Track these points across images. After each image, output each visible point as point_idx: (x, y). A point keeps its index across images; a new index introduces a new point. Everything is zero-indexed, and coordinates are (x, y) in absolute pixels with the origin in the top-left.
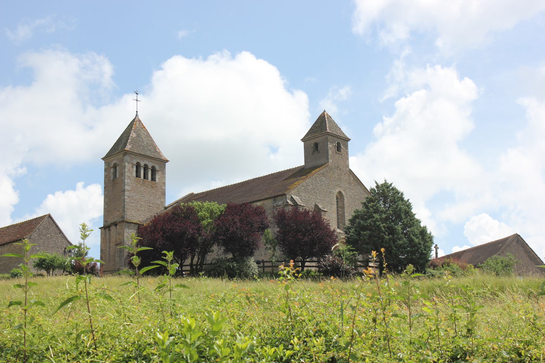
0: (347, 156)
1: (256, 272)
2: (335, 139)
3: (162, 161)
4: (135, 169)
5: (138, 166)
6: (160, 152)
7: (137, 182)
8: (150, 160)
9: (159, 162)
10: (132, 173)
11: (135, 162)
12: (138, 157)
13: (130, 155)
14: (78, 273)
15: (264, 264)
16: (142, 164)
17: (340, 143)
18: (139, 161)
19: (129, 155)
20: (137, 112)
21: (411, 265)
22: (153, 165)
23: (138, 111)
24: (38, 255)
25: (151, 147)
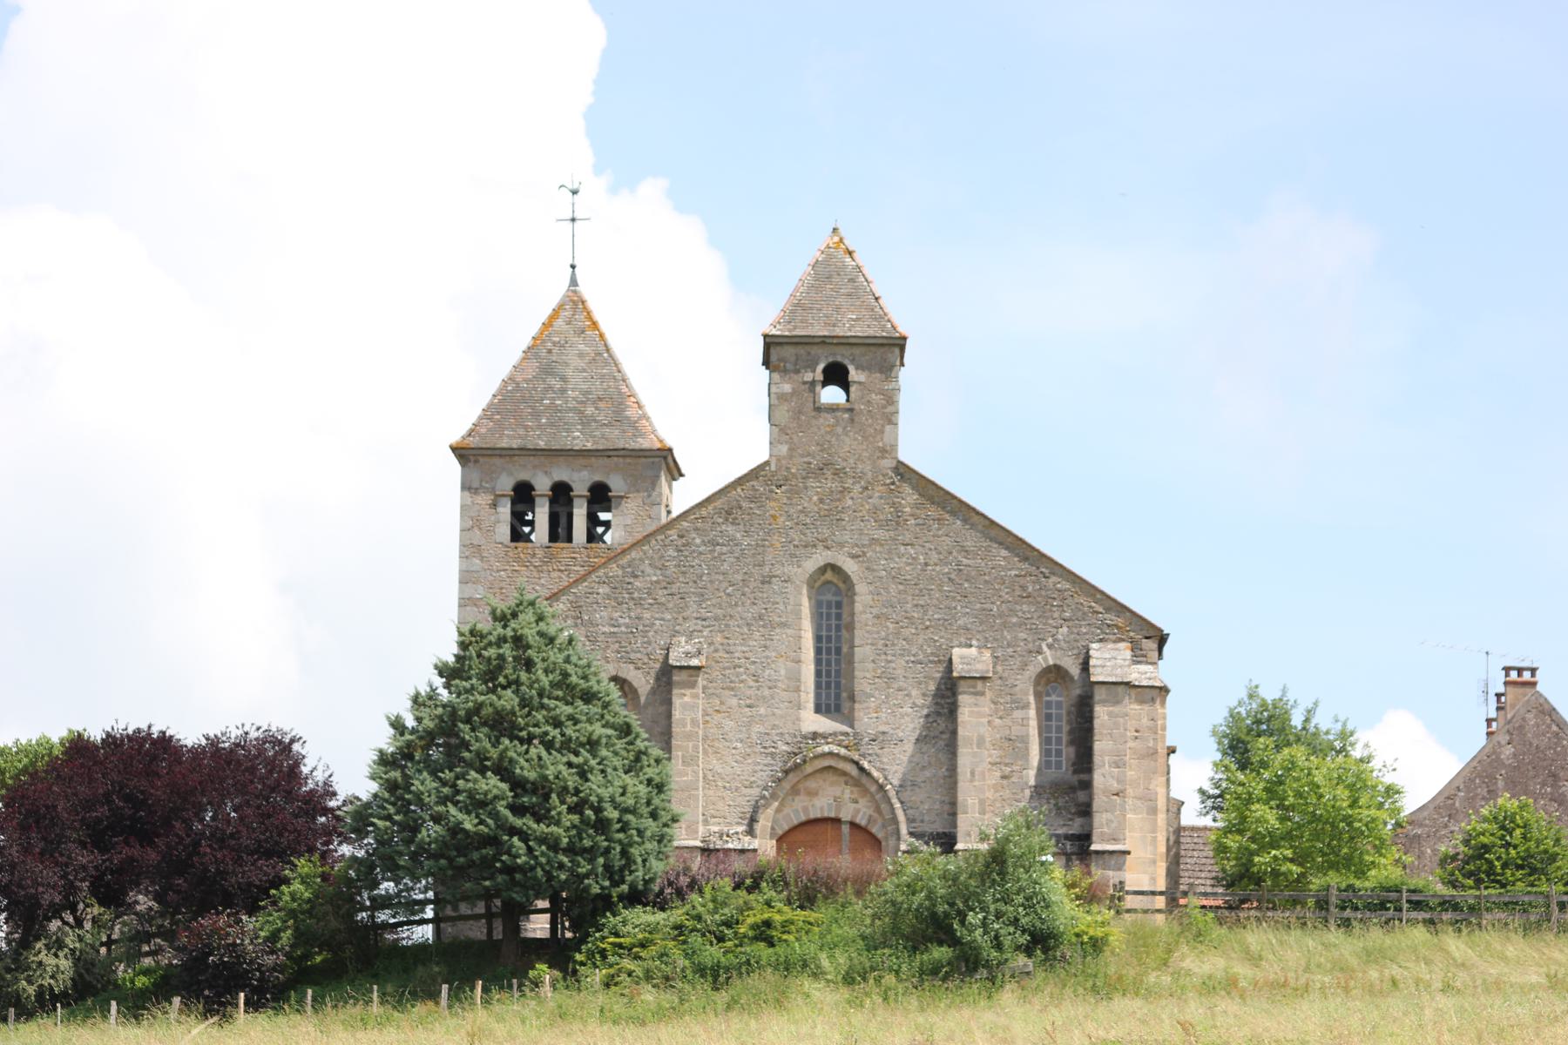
0: (890, 409)
1: (58, 986)
2: (815, 350)
3: (641, 453)
4: (505, 510)
5: (523, 495)
6: (645, 417)
7: (518, 560)
8: (582, 461)
9: (628, 460)
10: (491, 530)
11: (506, 484)
12: (522, 460)
13: (481, 460)
14: (1508, 751)
15: (488, 908)
16: (542, 485)
17: (846, 362)
18: (524, 476)
19: (476, 462)
20: (573, 267)
21: (544, 967)
22: (598, 478)
23: (576, 263)
24: (623, 781)
25: (601, 405)
